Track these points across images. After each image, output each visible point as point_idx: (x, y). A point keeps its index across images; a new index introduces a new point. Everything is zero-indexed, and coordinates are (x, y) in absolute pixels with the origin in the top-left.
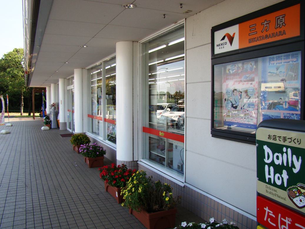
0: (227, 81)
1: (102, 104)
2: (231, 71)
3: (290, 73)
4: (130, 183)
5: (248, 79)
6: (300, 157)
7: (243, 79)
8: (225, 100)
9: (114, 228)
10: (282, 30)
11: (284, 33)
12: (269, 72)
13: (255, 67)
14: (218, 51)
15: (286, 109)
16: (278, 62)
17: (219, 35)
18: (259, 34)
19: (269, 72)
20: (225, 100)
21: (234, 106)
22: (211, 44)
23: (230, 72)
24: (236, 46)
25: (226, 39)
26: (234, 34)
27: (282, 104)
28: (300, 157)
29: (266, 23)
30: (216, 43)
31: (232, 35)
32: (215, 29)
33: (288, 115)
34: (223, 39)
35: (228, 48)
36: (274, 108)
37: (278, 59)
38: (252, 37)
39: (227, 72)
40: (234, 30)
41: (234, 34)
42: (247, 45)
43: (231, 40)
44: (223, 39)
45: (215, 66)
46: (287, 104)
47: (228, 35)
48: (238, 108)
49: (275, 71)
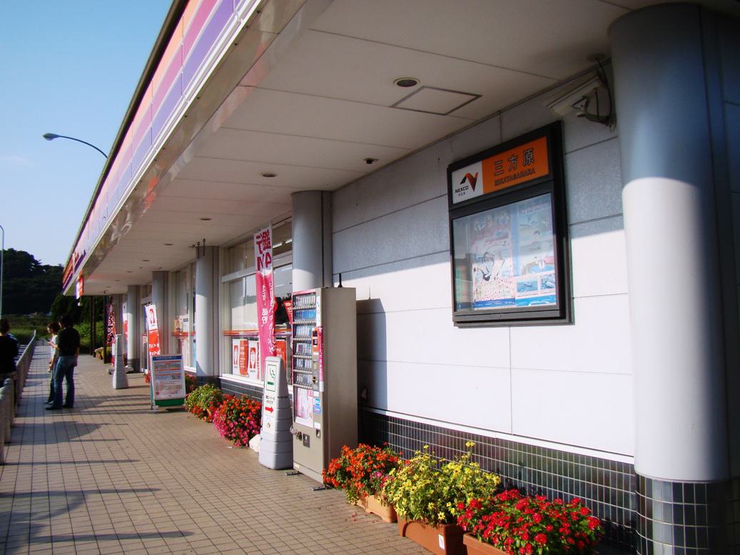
0: (476, 242)
1: (116, 362)
2: (479, 227)
3: (543, 222)
4: (477, 532)
5: (501, 235)
6: (65, 378)
7: (494, 236)
8: (475, 270)
9: (240, 552)
10: (530, 167)
11: (533, 171)
12: (522, 225)
13: (507, 218)
14: (457, 199)
15: (543, 270)
16: (529, 209)
17: (458, 176)
18: (518, 171)
19: (522, 225)
20: (475, 270)
21: (486, 276)
22: (74, 373)
23: (478, 229)
24: (479, 191)
25: (467, 183)
26: (477, 174)
27: (538, 265)
28: (65, 378)
29: (513, 158)
30: (454, 188)
31: (474, 176)
32: (454, 167)
33: (545, 277)
34: (463, 181)
35: (470, 194)
36: (529, 271)
37: (537, 203)
38: (500, 177)
39: (475, 229)
40: (476, 169)
41: (477, 174)
42: (493, 188)
43: (474, 183)
44: (463, 181)
45: (454, 221)
46: (543, 263)
47: (469, 176)
48: (284, 329)
49: (526, 223)
